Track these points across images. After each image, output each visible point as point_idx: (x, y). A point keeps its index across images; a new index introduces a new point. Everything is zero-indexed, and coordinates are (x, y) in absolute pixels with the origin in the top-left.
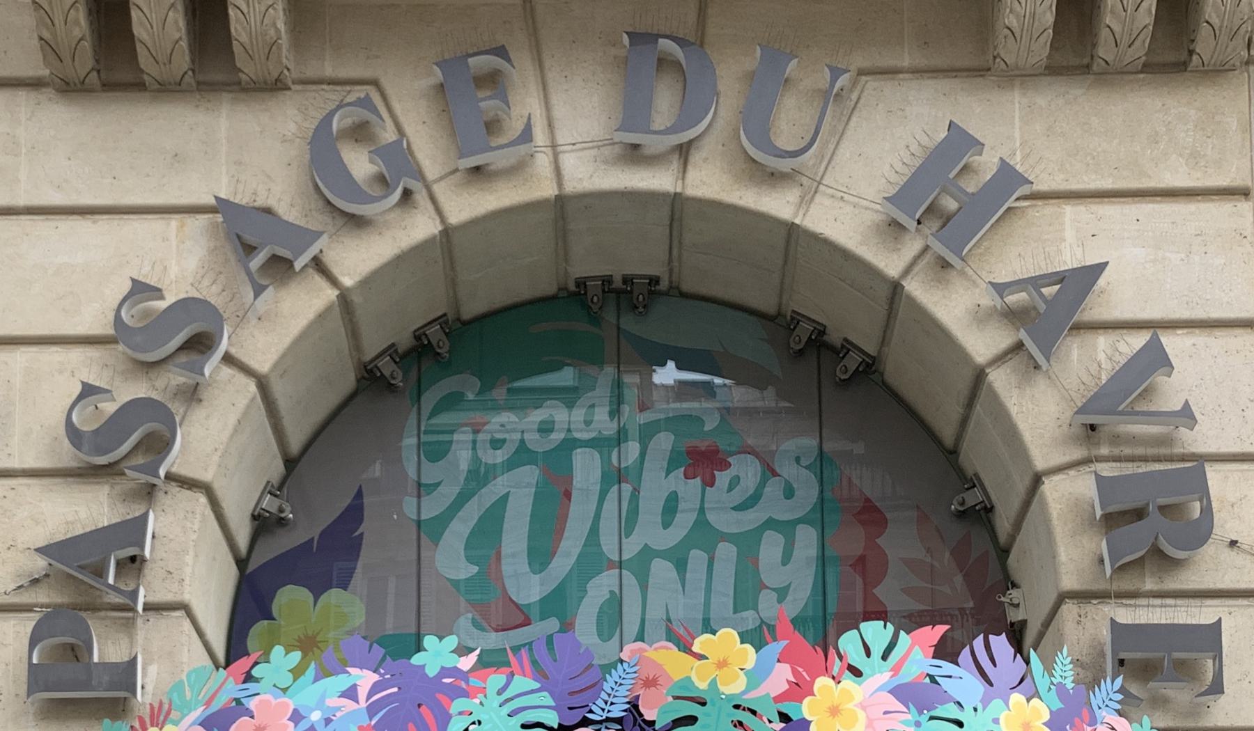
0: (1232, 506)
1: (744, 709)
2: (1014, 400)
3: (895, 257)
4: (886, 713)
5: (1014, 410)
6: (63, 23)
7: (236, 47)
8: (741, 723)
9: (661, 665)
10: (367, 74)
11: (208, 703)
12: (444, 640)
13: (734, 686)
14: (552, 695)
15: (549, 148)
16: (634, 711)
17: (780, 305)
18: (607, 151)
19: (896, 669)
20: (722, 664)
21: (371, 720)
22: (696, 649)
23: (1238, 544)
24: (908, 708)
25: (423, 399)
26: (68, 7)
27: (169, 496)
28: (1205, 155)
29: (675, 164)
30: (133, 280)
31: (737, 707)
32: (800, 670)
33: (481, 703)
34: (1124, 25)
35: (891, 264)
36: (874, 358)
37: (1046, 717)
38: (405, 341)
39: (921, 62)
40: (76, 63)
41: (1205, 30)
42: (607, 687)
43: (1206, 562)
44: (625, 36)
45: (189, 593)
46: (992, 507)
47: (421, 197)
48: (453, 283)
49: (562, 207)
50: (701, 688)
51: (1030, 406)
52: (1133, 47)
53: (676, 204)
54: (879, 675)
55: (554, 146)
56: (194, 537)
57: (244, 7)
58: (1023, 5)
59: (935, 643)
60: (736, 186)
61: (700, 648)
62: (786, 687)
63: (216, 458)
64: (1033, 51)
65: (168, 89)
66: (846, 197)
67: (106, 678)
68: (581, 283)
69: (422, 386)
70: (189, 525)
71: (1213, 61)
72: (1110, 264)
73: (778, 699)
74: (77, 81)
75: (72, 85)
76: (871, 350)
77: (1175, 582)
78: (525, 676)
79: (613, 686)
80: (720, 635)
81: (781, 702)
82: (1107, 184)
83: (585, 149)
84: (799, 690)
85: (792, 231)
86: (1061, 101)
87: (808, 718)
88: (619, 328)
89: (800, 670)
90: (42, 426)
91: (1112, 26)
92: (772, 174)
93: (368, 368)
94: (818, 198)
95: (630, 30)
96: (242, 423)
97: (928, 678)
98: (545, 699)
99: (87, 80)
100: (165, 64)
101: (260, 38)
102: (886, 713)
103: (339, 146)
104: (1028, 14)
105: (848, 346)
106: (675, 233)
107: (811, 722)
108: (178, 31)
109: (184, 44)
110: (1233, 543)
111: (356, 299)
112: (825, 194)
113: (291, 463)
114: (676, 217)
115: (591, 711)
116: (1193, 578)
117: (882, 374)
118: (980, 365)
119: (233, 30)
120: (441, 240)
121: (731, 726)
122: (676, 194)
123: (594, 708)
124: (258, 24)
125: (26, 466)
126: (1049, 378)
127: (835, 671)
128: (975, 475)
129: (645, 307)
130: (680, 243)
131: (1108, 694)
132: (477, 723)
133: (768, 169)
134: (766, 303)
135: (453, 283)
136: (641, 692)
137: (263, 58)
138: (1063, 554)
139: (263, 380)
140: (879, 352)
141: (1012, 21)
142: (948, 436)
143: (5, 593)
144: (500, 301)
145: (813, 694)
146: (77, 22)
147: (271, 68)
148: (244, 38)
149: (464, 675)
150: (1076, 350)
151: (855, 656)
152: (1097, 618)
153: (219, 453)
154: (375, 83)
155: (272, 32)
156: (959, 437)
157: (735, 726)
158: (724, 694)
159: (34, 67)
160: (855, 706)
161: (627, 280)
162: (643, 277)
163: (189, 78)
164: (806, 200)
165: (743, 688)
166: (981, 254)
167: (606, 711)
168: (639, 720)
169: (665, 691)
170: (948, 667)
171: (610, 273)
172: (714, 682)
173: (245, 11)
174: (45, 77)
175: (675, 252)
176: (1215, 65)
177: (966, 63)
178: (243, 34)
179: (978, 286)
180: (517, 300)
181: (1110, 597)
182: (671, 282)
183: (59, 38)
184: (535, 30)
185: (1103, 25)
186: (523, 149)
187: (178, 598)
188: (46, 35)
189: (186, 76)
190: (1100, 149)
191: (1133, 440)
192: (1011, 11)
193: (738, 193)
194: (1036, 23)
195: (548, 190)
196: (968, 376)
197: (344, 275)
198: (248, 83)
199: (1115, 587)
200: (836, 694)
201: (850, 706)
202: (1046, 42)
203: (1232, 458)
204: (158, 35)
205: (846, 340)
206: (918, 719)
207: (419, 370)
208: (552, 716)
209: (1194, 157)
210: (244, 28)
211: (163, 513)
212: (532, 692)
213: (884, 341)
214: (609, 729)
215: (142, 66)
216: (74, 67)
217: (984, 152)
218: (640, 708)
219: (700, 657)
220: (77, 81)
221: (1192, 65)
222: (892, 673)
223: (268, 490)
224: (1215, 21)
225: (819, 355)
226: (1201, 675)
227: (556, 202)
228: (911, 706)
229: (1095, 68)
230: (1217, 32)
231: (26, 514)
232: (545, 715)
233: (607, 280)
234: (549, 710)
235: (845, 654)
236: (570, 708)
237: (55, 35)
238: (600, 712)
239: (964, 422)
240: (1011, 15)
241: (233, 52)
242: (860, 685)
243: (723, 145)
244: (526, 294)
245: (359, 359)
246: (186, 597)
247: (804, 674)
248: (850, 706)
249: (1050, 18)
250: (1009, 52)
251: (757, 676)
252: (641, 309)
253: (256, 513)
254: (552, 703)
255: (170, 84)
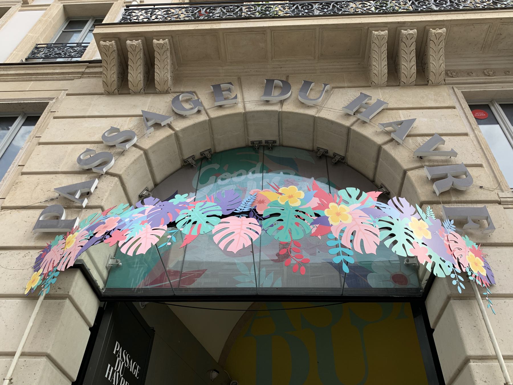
0: (477, 177)
1: (300, 212)
2: (393, 152)
3: (348, 121)
8: (299, 216)
11: (91, 224)
12: (182, 196)
13: (297, 204)
19: (363, 203)
20: (290, 197)
21: (147, 218)
22: (280, 191)
23: (483, 187)
24: (369, 216)
25: (201, 169)
26: (112, 74)
27: (106, 178)
34: (408, 73)
35: (347, 123)
38: (198, 156)
39: (350, 85)
40: (112, 87)
43: (473, 192)
45: (104, 203)
46: (389, 192)
47: (203, 112)
48: (213, 139)
52: (411, 78)
53: (280, 114)
55: (244, 102)
56: (111, 188)
57: (159, 73)
58: (378, 68)
60: (297, 109)
61: (282, 191)
62: (318, 205)
63: (124, 168)
64: (382, 79)
65: (136, 93)
66: (331, 110)
68: (253, 142)
69: (202, 166)
71: (435, 82)
72: (417, 119)
73: (313, 209)
74: (111, 92)
75: (110, 93)
76: (342, 154)
77: (463, 198)
78: (211, 202)
79: (246, 202)
80: (289, 188)
83: (252, 103)
85: (314, 118)
87: (328, 216)
88: (264, 154)
90: (72, 161)
91: (404, 73)
94: (322, 111)
95: (267, 79)
97: (376, 207)
100: (136, 87)
101: (162, 79)
104: (380, 70)
107: (328, 217)
108: (140, 78)
109: (142, 82)
110: (481, 187)
111: (180, 135)
112: (324, 110)
113: (156, 185)
114: (280, 120)
115: (236, 210)
116: (470, 197)
118: (379, 144)
119: (155, 78)
121: (295, 217)
122: (279, 112)
123: (237, 209)
124: (162, 76)
127: (338, 201)
128: (382, 184)
129: (271, 148)
131: (450, 225)
132: (189, 216)
133: (307, 105)
134: (308, 146)
135: (213, 139)
136: (257, 205)
137: (163, 85)
138: (419, 191)
140: (345, 154)
141: (375, 72)
142: (370, 175)
143: (40, 202)
145: (329, 208)
146: (113, 77)
147: (165, 87)
148: (158, 80)
150: (411, 140)
151: (346, 197)
152: (437, 209)
153: (126, 167)
154: (195, 92)
157: (296, 217)
159: (102, 90)
160: (347, 213)
161: (267, 142)
163: (142, 91)
164: (318, 112)
166: (375, 120)
168: (256, 214)
169: (267, 205)
170: (383, 205)
171: (261, 140)
173: (159, 74)
175: (280, 133)
176: (436, 83)
178: (158, 79)
182: (280, 143)
183: (108, 81)
184: (241, 82)
186: (234, 101)
188: (105, 80)
189: (141, 90)
190: (407, 100)
192: (374, 61)
193: (298, 110)
194: (382, 72)
195: (242, 111)
196: (375, 149)
199: (441, 200)
200: (339, 209)
201: (345, 213)
202: (386, 77)
203: (472, 166)
204: (135, 79)
206: (374, 220)
207: (201, 163)
208: (220, 213)
209: (436, 101)
211: (102, 182)
212: (213, 206)
213: (346, 151)
214: (243, 216)
215: (129, 87)
217: (372, 99)
218: (257, 210)
219: (281, 194)
220: (111, 92)
223: (146, 189)
226: (483, 226)
229: (401, 84)
231: (57, 182)
232: (218, 213)
233: (260, 142)
234: (219, 211)
235: (341, 196)
239: (376, 168)
240: (375, 71)
241: (155, 83)
242: (348, 206)
243: (293, 101)
244: (236, 146)
245: (182, 158)
246: (102, 204)
247: (325, 201)
248: (345, 213)
250: (375, 80)
251: (306, 200)
252: (271, 149)
255: (137, 93)
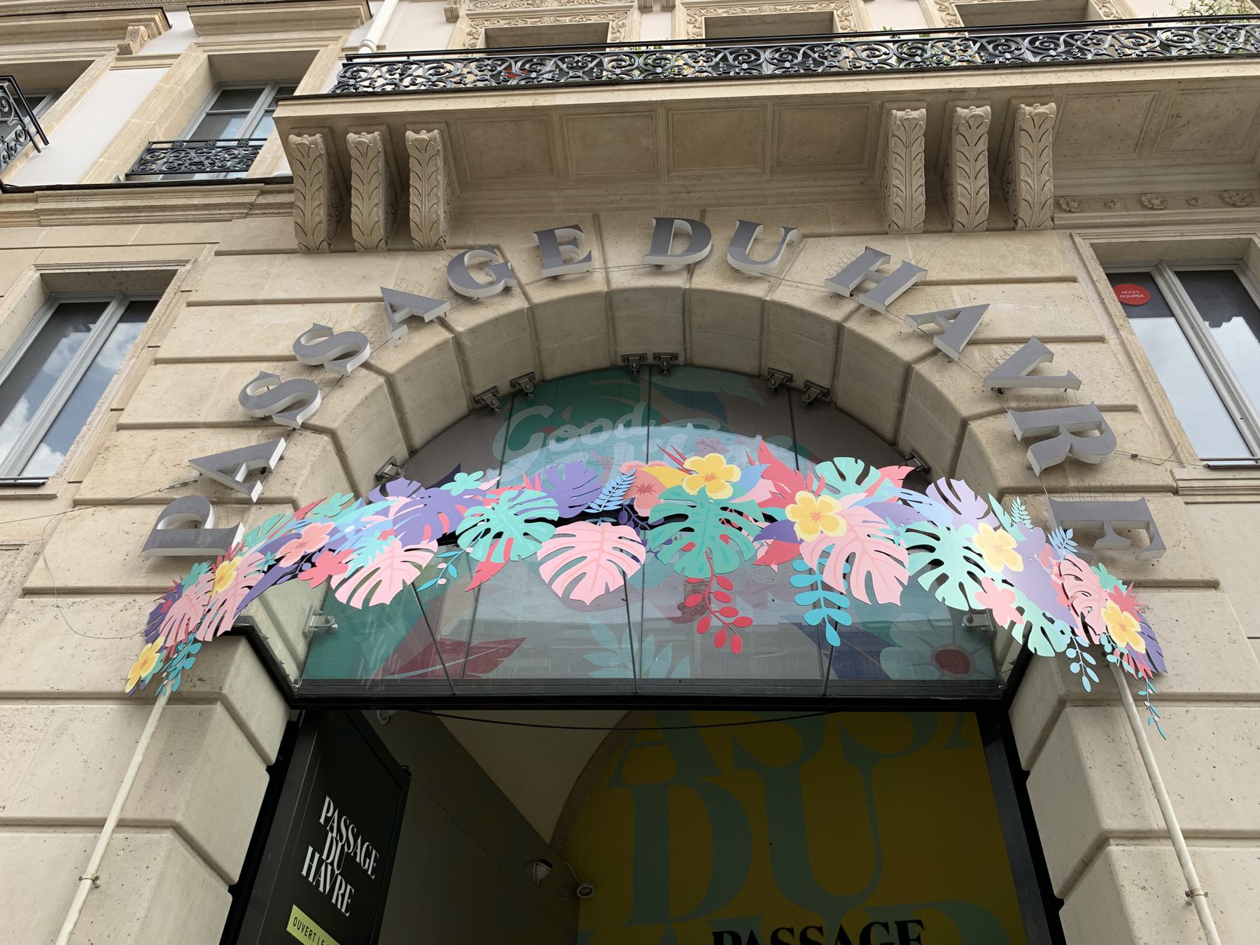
1: (731, 511)
2: (937, 378)
4: (864, 522)
5: (938, 384)
6: (310, 214)
7: (412, 225)
8: (728, 521)
9: (656, 477)
10: (493, 243)
11: (270, 537)
13: (724, 493)
14: (556, 500)
15: (603, 270)
16: (629, 510)
17: (760, 367)
18: (641, 271)
19: (871, 492)
20: (710, 478)
21: (394, 526)
22: (687, 465)
25: (512, 418)
27: (302, 436)
28: (1040, 264)
29: (685, 275)
30: (314, 324)
31: (724, 509)
32: (782, 485)
33: (493, 509)
35: (836, 314)
36: (829, 390)
37: (1015, 545)
39: (840, 229)
41: (1023, 204)
42: (605, 491)
44: (654, 220)
46: (930, 468)
47: (517, 290)
48: (538, 351)
49: (610, 301)
50: (691, 494)
51: (949, 381)
53: (686, 298)
54: (855, 494)
55: (606, 269)
58: (904, 192)
59: (904, 478)
60: (725, 283)
65: (370, 250)
67: (209, 539)
68: (626, 358)
69: (514, 411)
70: (312, 452)
71: (1032, 224)
73: (761, 505)
81: (766, 506)
82: (978, 276)
84: (783, 499)
86: (937, 244)
87: (792, 520)
89: (782, 485)
92: (749, 278)
93: (476, 399)
96: (369, 399)
98: (552, 503)
99: (321, 247)
100: (368, 235)
101: (427, 219)
102: (864, 522)
103: (469, 271)
104: (908, 197)
105: (809, 385)
106: (687, 319)
107: (794, 523)
110: (1134, 457)
111: (467, 342)
116: (1108, 478)
117: (835, 403)
120: (527, 313)
121: (720, 523)
125: (208, 420)
126: (961, 367)
129: (667, 370)
130: (690, 327)
134: (749, 365)
135: (538, 351)
136: (636, 496)
139: (390, 378)
140: (832, 385)
144: (571, 368)
146: (319, 214)
148: (417, 220)
149: (483, 493)
153: (347, 413)
154: (498, 247)
155: (435, 216)
156: (897, 429)
157: (723, 523)
158: (711, 499)
159: (294, 244)
162: (667, 354)
163: (382, 244)
164: (771, 289)
165: (730, 495)
166: (898, 309)
167: (602, 507)
168: (633, 516)
169: (658, 496)
170: (916, 495)
172: (703, 490)
174: (296, 249)
175: (688, 336)
176: (1033, 226)
177: (871, 230)
179: (898, 324)
180: (582, 369)
181: (1044, 493)
182: (686, 359)
184: (599, 226)
185: (957, 203)
186: (585, 266)
187: (288, 495)
188: (299, 221)
189: (380, 243)
191: (1036, 398)
194: (914, 201)
196: (898, 373)
197: (457, 326)
198: (418, 247)
199: (1044, 484)
201: (831, 514)
205: (807, 381)
208: (554, 513)
209: (1033, 265)
210: (418, 215)
212: (539, 498)
213: (834, 375)
216: (314, 239)
219: (688, 472)
221: (1018, 227)
222: (866, 494)
224: (1030, 199)
225: (789, 394)
227: (606, 296)
228: (888, 519)
230: (1032, 205)
231: (196, 446)
233: (642, 357)
236: (570, 507)
237: (304, 223)
238: (598, 508)
242: (838, 499)
246: (295, 495)
247: (786, 488)
248: (831, 514)
249: (922, 199)
251: (744, 485)
252: (665, 372)
253: (378, 474)
254: (557, 505)
